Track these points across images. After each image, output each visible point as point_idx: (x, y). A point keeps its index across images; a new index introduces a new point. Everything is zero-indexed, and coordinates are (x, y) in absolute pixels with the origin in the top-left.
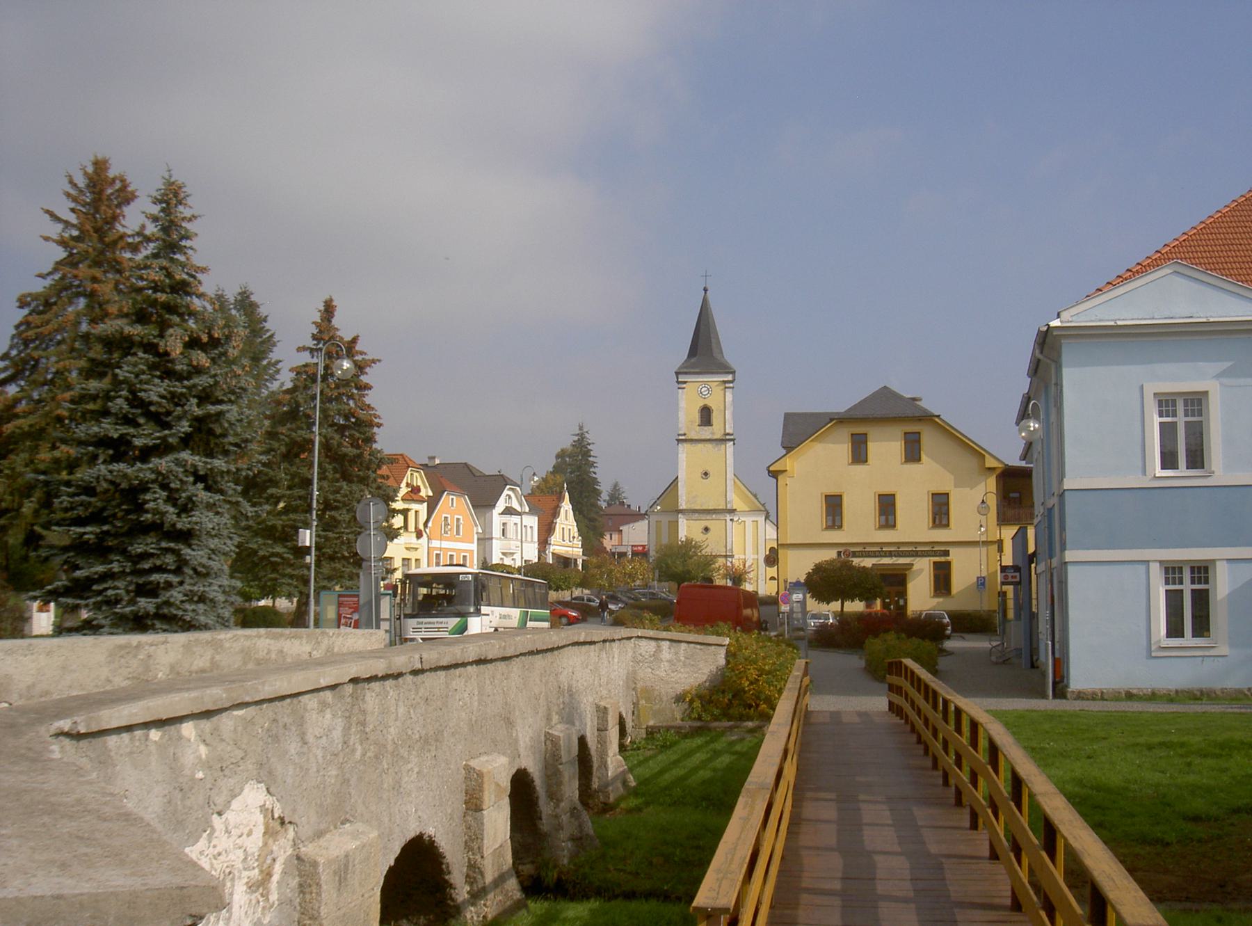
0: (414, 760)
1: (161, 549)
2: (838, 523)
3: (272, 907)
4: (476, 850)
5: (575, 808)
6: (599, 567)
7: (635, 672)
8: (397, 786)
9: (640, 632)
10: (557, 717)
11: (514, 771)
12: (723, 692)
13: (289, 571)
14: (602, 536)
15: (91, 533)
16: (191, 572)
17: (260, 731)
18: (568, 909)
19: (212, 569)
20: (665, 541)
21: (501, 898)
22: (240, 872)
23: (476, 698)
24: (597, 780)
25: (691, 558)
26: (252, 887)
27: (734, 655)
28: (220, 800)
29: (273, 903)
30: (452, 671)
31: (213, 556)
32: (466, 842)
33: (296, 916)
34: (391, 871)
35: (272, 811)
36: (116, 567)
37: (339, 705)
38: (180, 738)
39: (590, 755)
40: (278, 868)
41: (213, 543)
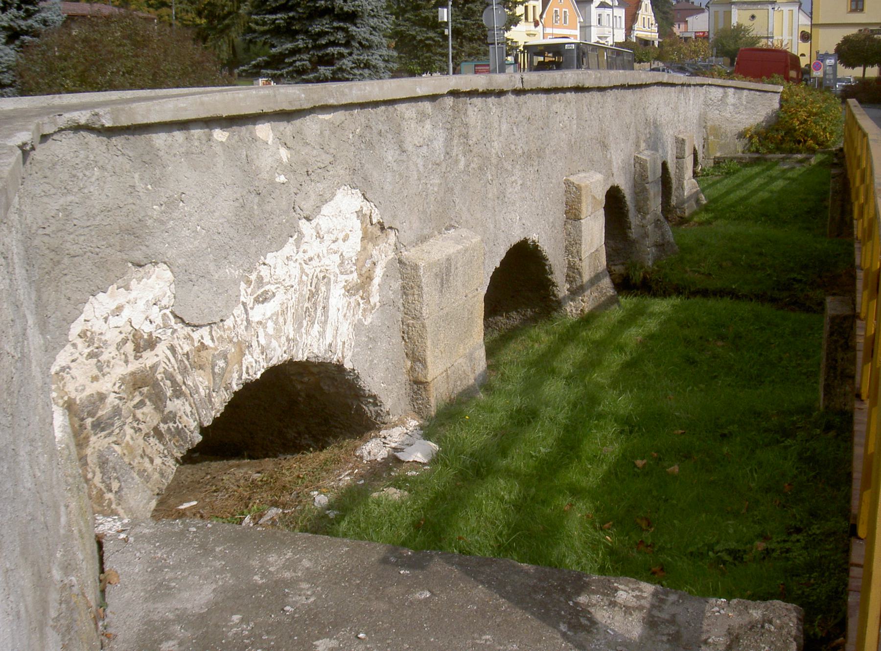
0: (517, 172)
1: (334, 28)
2: (860, 7)
3: (373, 308)
4: (575, 254)
5: (658, 220)
6: (671, 45)
7: (705, 114)
8: (501, 196)
9: (710, 81)
10: (644, 144)
11: (608, 187)
12: (777, 130)
13: (439, 50)
14: (672, 25)
15: (281, 18)
16: (357, 45)
17: (351, 136)
18: (653, 304)
19: (373, 42)
20: (721, 26)
21: (596, 294)
22: (336, 275)
23: (575, 122)
24: (675, 198)
25: (741, 39)
26: (350, 290)
27: (786, 101)
28: (307, 206)
29: (375, 305)
30: (552, 95)
31: (374, 32)
32: (566, 247)
33: (400, 316)
34: (497, 271)
35: (370, 217)
36: (301, 44)
37: (440, 117)
38: (255, 139)
39: (670, 178)
40: (379, 272)
41: (373, 22)
